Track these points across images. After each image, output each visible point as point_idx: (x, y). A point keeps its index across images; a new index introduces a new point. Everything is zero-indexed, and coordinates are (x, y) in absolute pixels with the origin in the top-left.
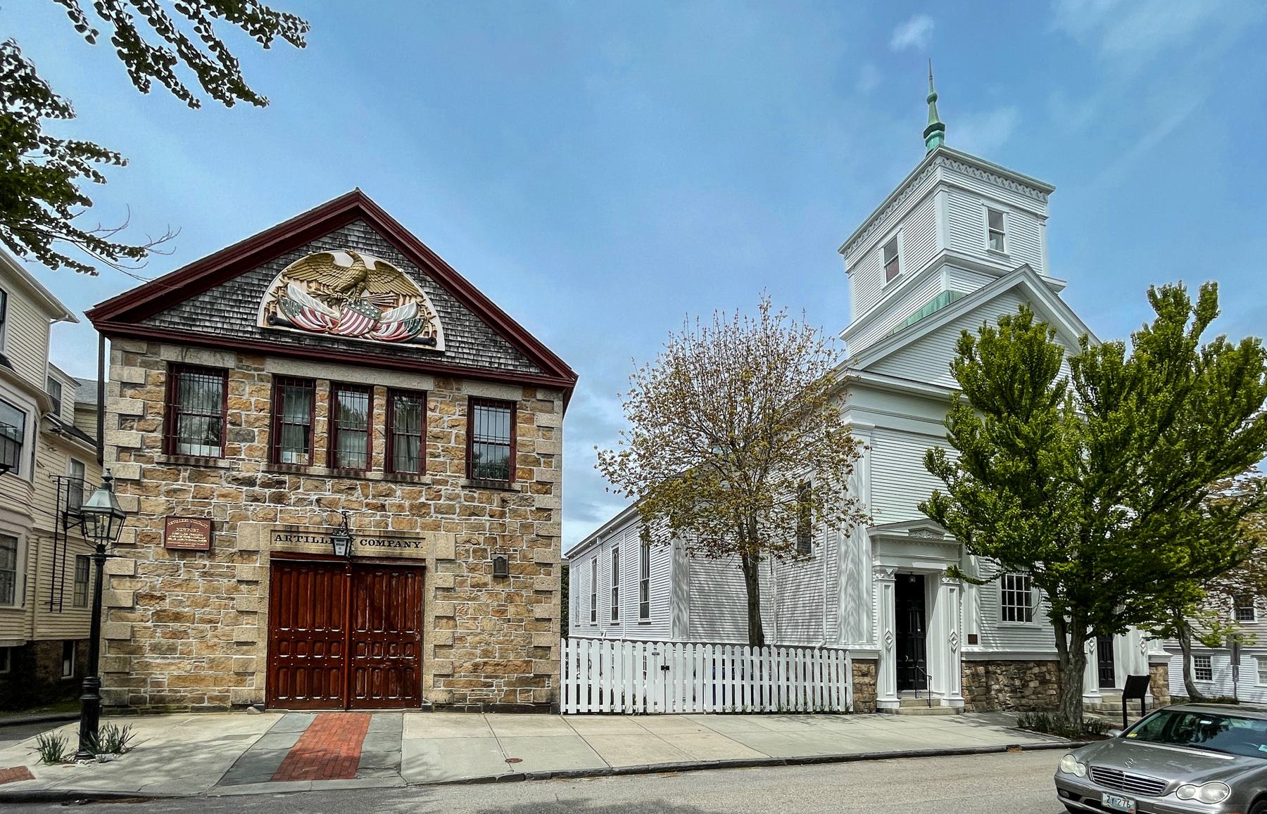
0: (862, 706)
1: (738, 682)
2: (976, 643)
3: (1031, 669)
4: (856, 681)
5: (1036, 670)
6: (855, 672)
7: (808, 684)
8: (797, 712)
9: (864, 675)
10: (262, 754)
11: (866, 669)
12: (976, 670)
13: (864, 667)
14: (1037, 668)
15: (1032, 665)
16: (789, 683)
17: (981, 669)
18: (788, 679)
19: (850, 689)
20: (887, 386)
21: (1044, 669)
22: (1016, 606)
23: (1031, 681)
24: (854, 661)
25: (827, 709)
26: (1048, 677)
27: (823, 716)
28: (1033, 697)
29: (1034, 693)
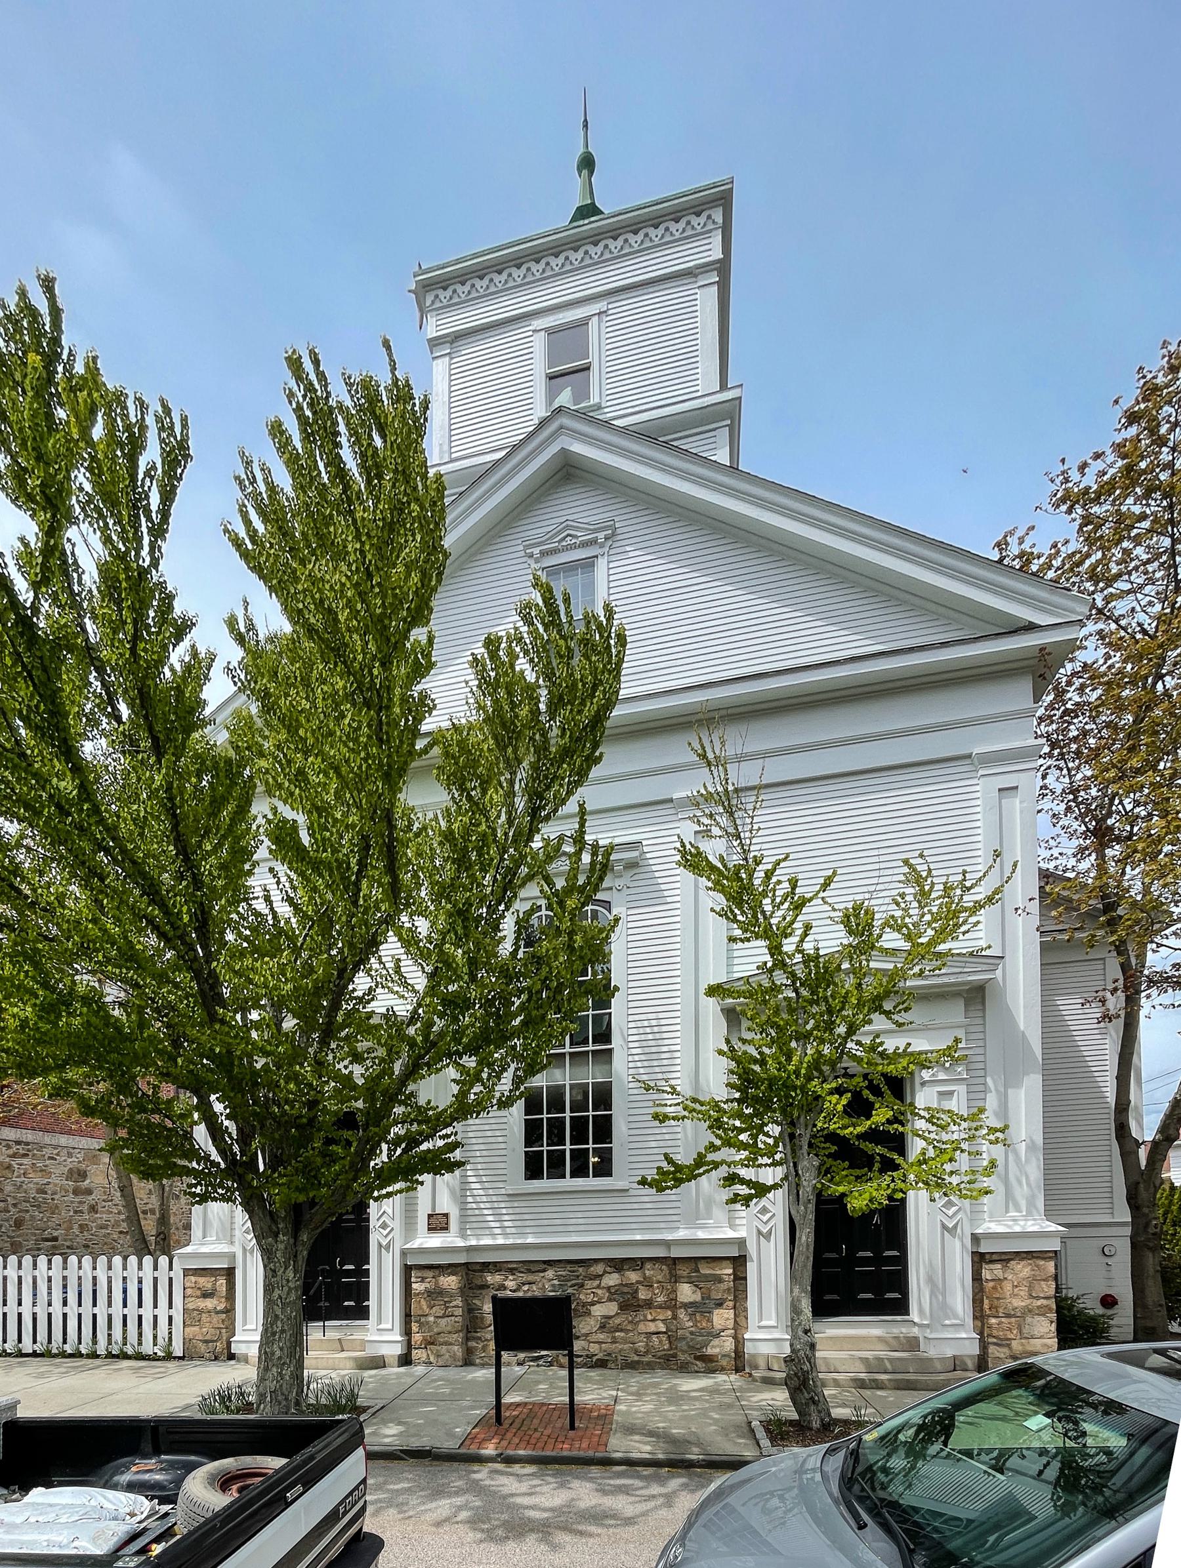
0: (202, 1347)
1: (147, 1312)
2: (445, 1228)
3: (600, 1277)
4: (191, 1306)
5: (612, 1280)
6: (189, 1291)
7: (101, 1311)
8: (77, 1355)
9: (206, 1295)
10: (531, 1475)
11: (209, 1286)
12: (437, 1283)
13: (205, 1282)
14: (616, 1276)
15: (599, 1269)
16: (67, 1310)
17: (450, 1282)
18: (65, 1303)
19: (178, 1319)
20: (770, 696)
21: (633, 1276)
22: (568, 1147)
23: (593, 1304)
24: (187, 1272)
25: (129, 1350)
26: (643, 1295)
27: (171, 1365)
28: (601, 1336)
29: (603, 1327)
